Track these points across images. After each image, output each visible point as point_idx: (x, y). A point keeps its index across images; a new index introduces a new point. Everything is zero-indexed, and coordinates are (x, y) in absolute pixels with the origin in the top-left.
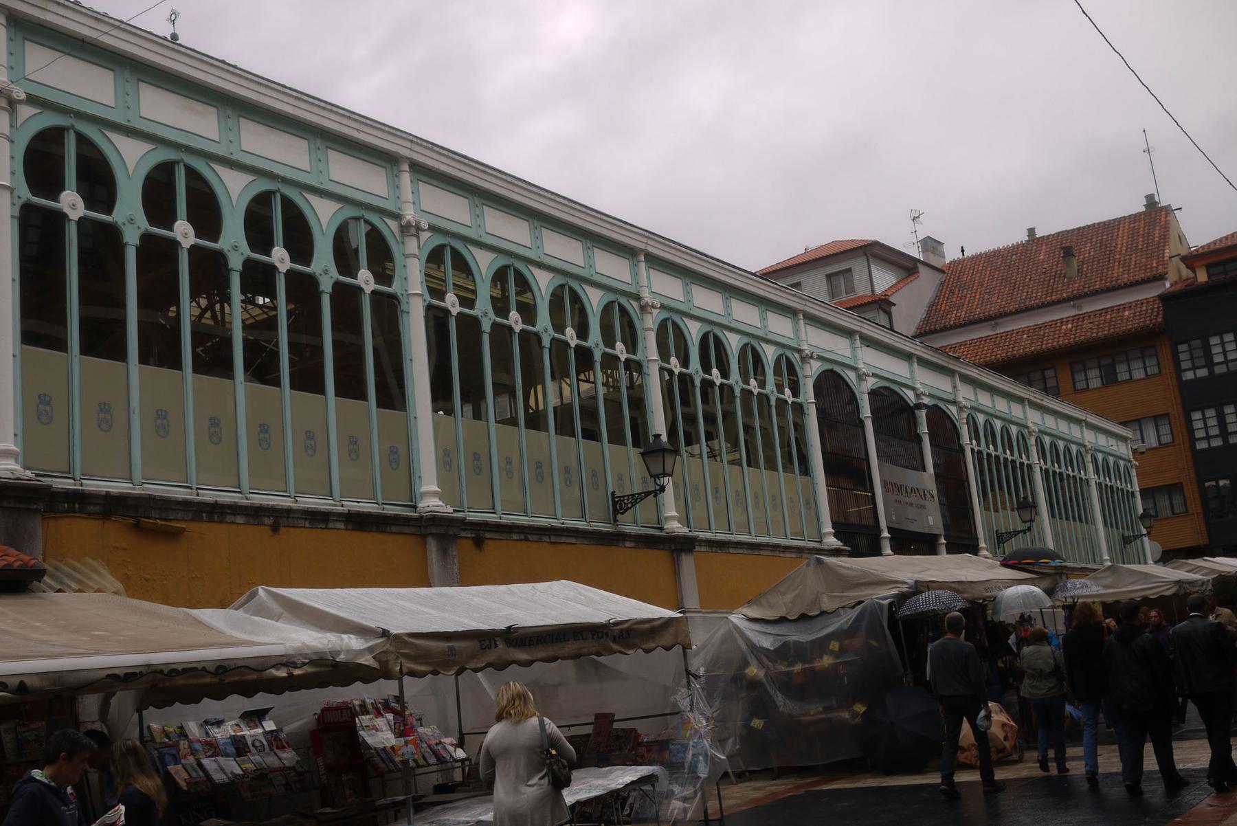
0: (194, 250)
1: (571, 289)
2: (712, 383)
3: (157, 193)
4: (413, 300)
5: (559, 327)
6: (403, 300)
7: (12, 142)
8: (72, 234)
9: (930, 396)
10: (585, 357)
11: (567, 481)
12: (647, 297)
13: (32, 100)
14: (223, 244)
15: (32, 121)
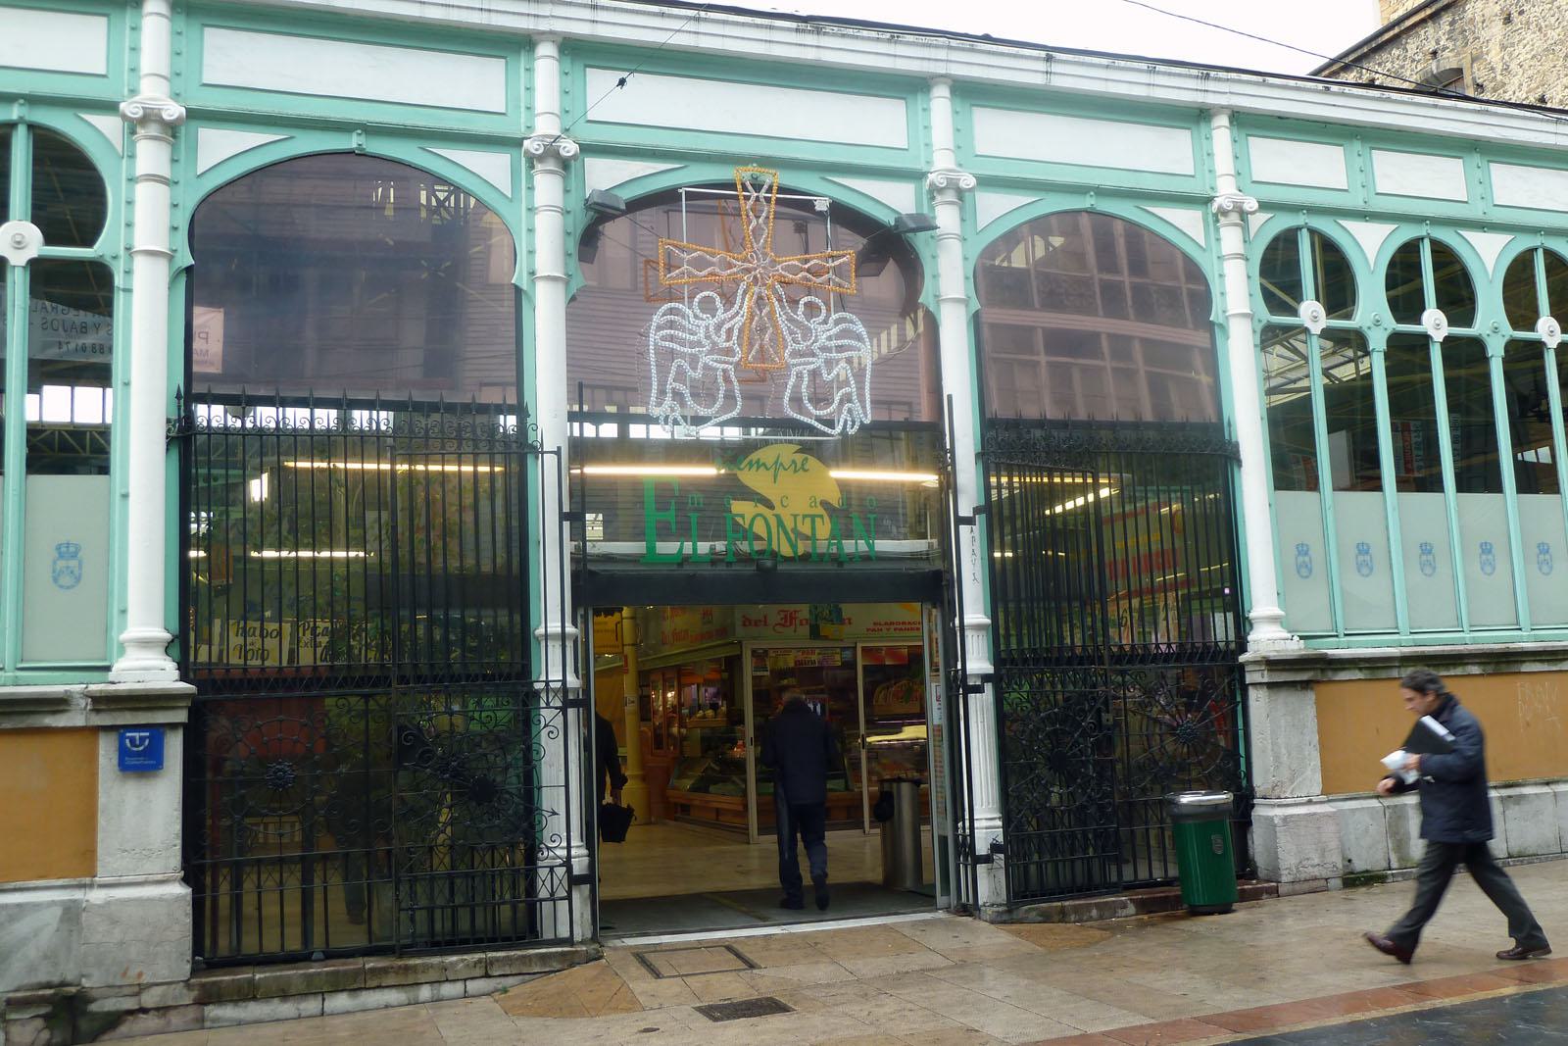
4: (140, 264)
7: (1247, 260)
13: (1264, 206)
14: (1479, 327)
15: (1267, 227)
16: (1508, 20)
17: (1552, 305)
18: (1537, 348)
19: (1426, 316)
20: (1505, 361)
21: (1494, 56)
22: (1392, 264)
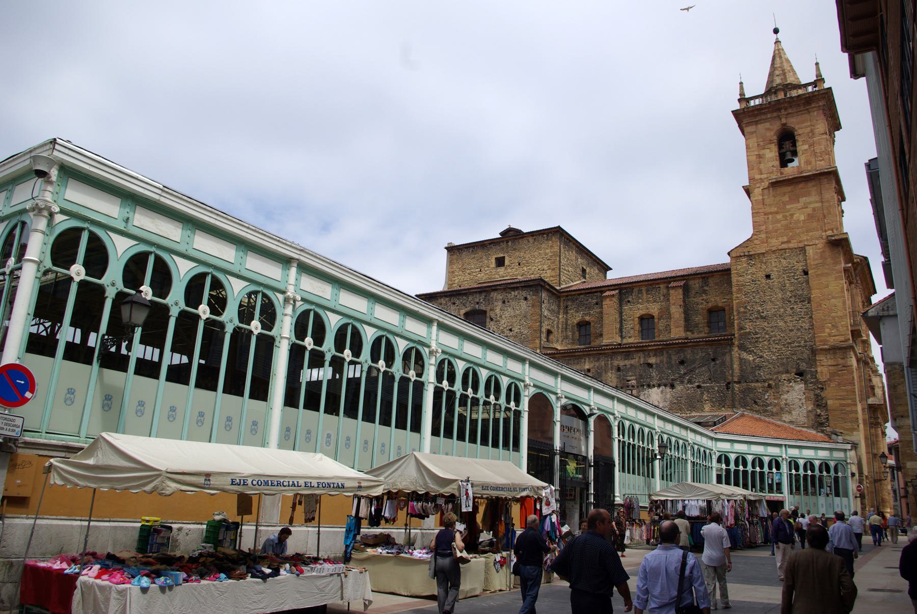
0: (82, 284)
1: (387, 338)
2: (467, 396)
3: (134, 269)
5: (465, 388)
6: (277, 340)
8: (254, 340)
9: (599, 409)
10: (475, 402)
11: (365, 448)
12: (528, 381)
13: (63, 212)
14: (324, 348)
15: (302, 307)
16: (504, 302)
17: (152, 281)
19: (253, 322)
21: (498, 311)
22: (338, 330)
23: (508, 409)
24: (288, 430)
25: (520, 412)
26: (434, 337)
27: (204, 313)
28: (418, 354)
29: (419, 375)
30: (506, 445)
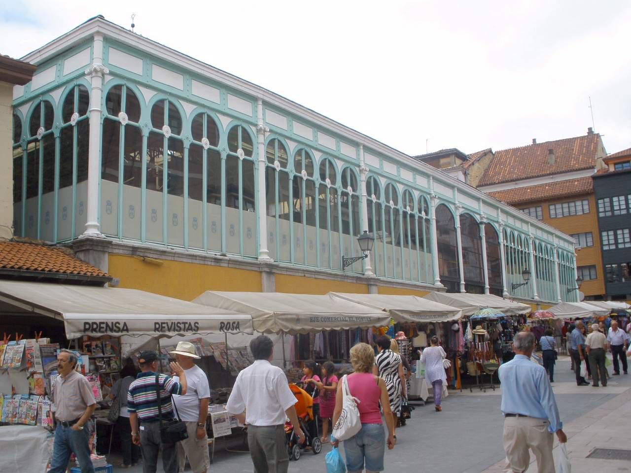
7: (102, 91)
11: (323, 250)
13: (111, 73)
18: (117, 124)
19: (203, 139)
20: (149, 138)
23: (345, 194)
24: (109, 203)
25: (252, 163)
26: (260, 115)
27: (124, 119)
28: (245, 133)
29: (248, 153)
30: (232, 201)
